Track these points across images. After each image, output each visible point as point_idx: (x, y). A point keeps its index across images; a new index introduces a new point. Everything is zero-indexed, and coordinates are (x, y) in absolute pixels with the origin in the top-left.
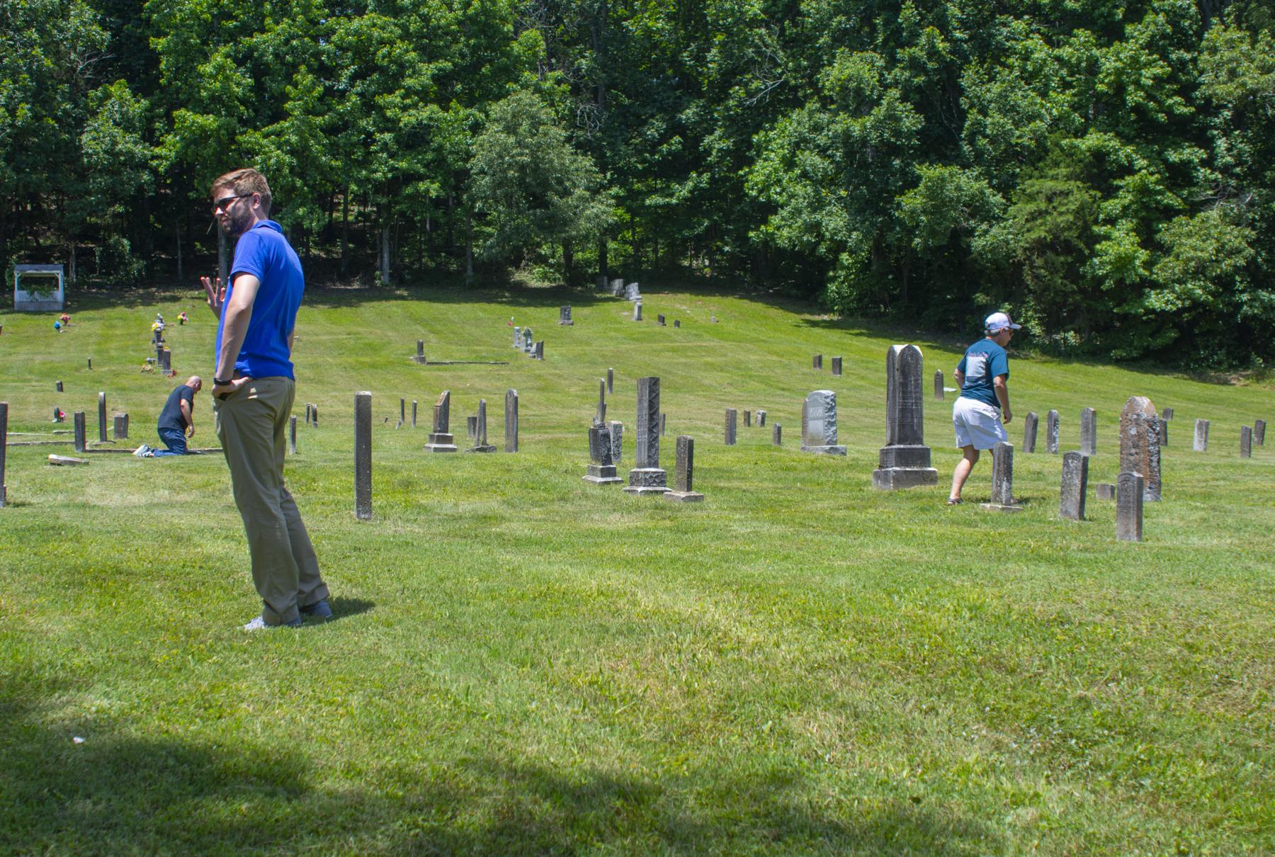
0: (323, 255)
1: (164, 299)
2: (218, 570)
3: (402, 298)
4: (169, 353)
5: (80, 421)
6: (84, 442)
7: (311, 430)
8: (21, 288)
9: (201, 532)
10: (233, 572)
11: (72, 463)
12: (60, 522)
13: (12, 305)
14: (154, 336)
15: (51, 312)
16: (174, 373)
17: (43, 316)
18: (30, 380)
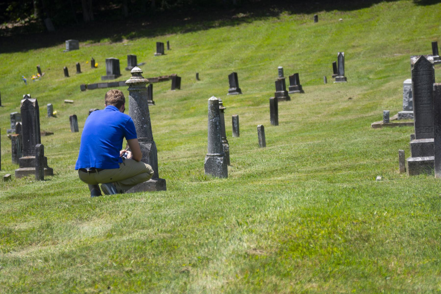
3: (243, 20)
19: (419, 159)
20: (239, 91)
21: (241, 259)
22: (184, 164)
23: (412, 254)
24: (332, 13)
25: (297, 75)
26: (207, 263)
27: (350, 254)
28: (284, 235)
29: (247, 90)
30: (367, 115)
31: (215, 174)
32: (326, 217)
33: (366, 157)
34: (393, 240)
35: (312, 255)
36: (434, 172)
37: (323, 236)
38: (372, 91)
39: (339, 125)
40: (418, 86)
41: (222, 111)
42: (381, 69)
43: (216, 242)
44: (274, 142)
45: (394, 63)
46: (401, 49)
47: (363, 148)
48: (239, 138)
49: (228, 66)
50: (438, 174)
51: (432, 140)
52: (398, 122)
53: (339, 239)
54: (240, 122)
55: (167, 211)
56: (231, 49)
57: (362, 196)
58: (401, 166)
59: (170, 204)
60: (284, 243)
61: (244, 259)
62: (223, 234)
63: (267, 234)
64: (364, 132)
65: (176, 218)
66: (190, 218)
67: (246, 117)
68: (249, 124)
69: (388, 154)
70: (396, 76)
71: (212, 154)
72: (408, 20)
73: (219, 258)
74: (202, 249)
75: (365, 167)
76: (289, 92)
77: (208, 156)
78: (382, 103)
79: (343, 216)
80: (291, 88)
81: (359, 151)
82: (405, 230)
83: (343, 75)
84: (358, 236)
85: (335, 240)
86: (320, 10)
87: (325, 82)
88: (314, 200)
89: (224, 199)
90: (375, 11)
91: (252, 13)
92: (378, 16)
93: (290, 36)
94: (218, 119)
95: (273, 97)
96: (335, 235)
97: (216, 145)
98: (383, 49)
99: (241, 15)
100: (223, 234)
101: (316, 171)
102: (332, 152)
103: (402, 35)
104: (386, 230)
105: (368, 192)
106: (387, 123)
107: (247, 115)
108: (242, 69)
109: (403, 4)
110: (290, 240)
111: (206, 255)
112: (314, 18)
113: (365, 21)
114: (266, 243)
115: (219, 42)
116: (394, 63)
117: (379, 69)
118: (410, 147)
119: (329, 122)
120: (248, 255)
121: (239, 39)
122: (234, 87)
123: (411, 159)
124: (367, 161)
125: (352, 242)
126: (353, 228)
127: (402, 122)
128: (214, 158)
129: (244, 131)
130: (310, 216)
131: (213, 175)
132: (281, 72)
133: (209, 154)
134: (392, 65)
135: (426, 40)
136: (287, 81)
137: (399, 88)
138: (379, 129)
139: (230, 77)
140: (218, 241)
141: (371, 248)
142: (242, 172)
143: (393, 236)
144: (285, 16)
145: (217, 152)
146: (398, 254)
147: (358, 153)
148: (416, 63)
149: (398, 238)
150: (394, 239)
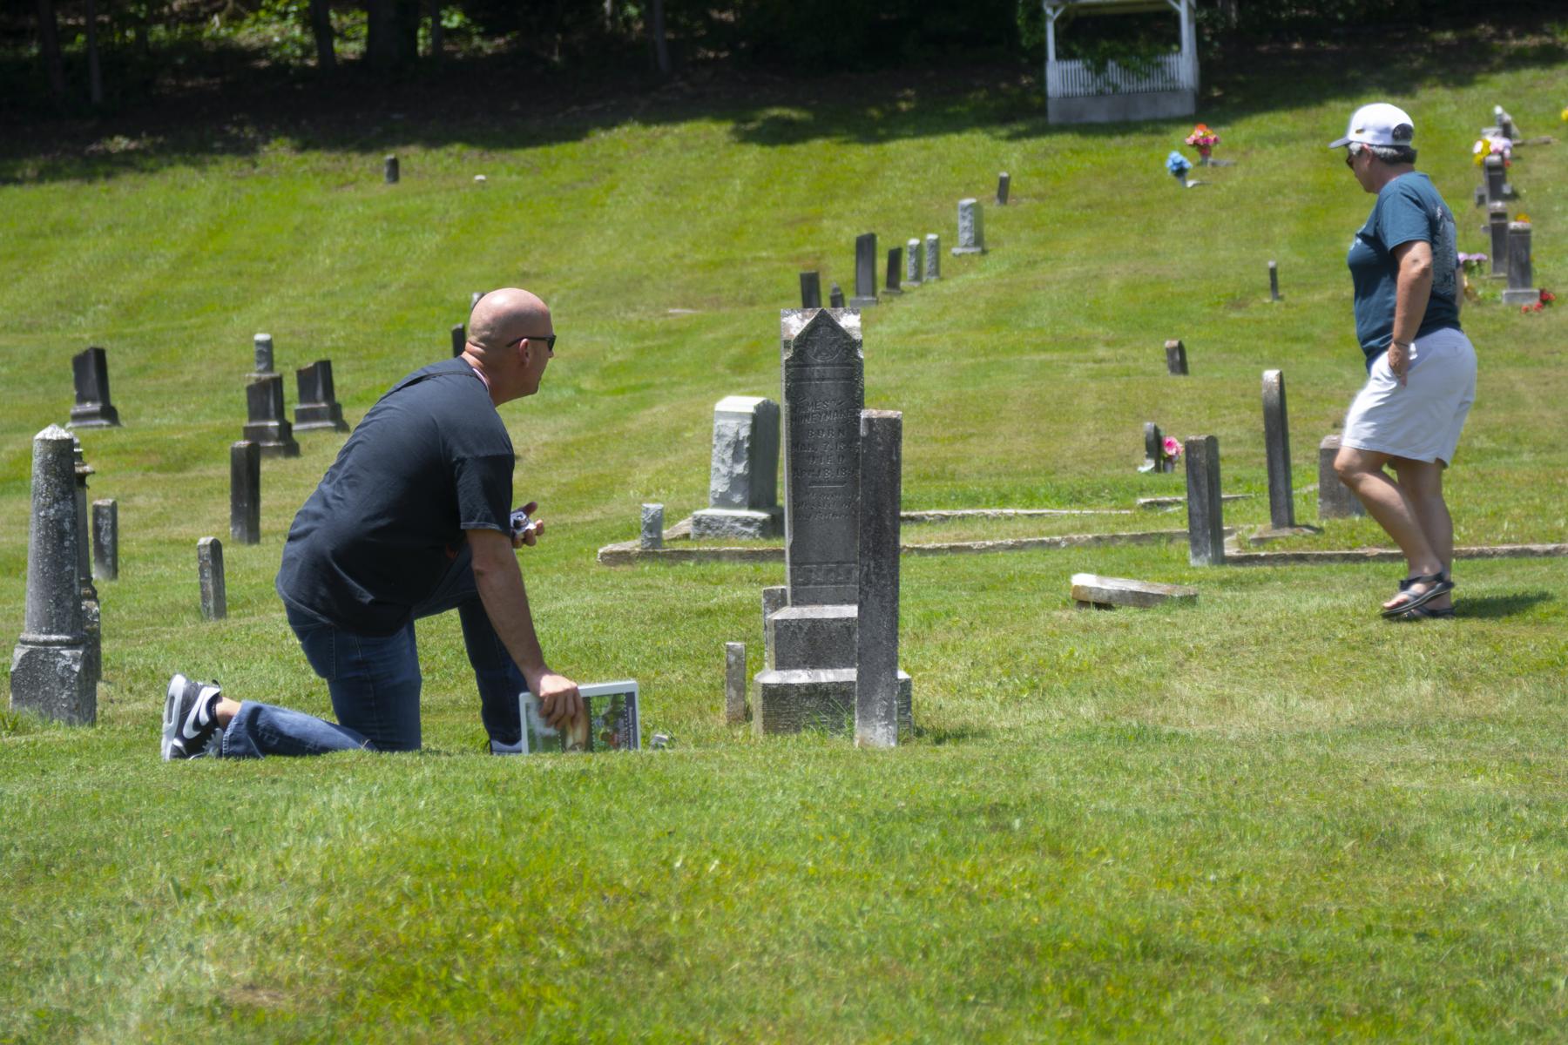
0: (715, 14)
1: (1518, 61)
2: (1479, 946)
3: (126, 162)
4: (1523, 236)
5: (1204, 467)
6: (1217, 536)
7: (248, 550)
8: (1064, 54)
9: (1460, 816)
10: (1525, 954)
11: (1142, 600)
12: (1027, 788)
13: (1042, 111)
14: (1481, 182)
15: (1158, 125)
16: (1545, 299)
17: (1135, 140)
18: (1083, 343)
19: (801, 677)
20: (109, 413)
21: (199, 1022)
23: (829, 1014)
24: (450, 155)
25: (325, 367)
26: (71, 1035)
27: (607, 1010)
28: (356, 937)
29: (138, 413)
30: (579, 519)
31: (49, 708)
32: (501, 875)
34: (754, 964)
35: (465, 1010)
36: (851, 724)
37: (499, 945)
38: (590, 434)
40: (807, 416)
41: (82, 478)
42: (620, 358)
43: (97, 957)
44: (249, 602)
45: (665, 341)
46: (691, 292)
48: (115, 584)
49: (69, 324)
50: (868, 731)
51: (851, 611)
53: (557, 956)
54: (120, 523)
56: (79, 265)
57: (618, 801)
58: (732, 701)
60: (358, 967)
61: (212, 1023)
62: (124, 929)
63: (288, 932)
64: (574, 576)
67: (138, 509)
68: (151, 534)
69: (676, 657)
70: (673, 384)
71: (43, 638)
72: (716, 192)
73: (116, 1017)
74: (47, 981)
76: (295, 427)
77: (25, 642)
78: (630, 479)
79: (564, 871)
80: (303, 410)
81: (572, 644)
82: (793, 928)
84: (626, 944)
85: (545, 958)
86: (406, 143)
88: (448, 813)
90: (602, 155)
91: (160, 139)
92: (610, 171)
93: (297, 229)
95: (243, 443)
96: (542, 939)
97: (59, 602)
98: (630, 287)
99: (122, 143)
100: (124, 929)
103: (696, 245)
104: (726, 925)
105: (638, 787)
106: (656, 552)
107: (140, 501)
108: (122, 337)
109: (697, 137)
110: (379, 956)
111: (66, 1006)
112: (386, 170)
113: (563, 186)
114: (288, 963)
116: (665, 341)
117: (612, 358)
118: (772, 633)
120: (224, 1007)
122: (93, 400)
125: (608, 967)
126: (607, 917)
128: (47, 652)
129: (132, 558)
131: (41, 715)
132: (266, 352)
133: (31, 637)
134: (659, 348)
135: (777, 265)
136: (291, 388)
137: (686, 429)
138: (624, 569)
139: (80, 362)
140: (106, 956)
141: (679, 988)
143: (753, 946)
144: (279, 154)
145: (61, 631)
146: (777, 1012)
147: (568, 649)
149: (771, 954)
150: (758, 956)
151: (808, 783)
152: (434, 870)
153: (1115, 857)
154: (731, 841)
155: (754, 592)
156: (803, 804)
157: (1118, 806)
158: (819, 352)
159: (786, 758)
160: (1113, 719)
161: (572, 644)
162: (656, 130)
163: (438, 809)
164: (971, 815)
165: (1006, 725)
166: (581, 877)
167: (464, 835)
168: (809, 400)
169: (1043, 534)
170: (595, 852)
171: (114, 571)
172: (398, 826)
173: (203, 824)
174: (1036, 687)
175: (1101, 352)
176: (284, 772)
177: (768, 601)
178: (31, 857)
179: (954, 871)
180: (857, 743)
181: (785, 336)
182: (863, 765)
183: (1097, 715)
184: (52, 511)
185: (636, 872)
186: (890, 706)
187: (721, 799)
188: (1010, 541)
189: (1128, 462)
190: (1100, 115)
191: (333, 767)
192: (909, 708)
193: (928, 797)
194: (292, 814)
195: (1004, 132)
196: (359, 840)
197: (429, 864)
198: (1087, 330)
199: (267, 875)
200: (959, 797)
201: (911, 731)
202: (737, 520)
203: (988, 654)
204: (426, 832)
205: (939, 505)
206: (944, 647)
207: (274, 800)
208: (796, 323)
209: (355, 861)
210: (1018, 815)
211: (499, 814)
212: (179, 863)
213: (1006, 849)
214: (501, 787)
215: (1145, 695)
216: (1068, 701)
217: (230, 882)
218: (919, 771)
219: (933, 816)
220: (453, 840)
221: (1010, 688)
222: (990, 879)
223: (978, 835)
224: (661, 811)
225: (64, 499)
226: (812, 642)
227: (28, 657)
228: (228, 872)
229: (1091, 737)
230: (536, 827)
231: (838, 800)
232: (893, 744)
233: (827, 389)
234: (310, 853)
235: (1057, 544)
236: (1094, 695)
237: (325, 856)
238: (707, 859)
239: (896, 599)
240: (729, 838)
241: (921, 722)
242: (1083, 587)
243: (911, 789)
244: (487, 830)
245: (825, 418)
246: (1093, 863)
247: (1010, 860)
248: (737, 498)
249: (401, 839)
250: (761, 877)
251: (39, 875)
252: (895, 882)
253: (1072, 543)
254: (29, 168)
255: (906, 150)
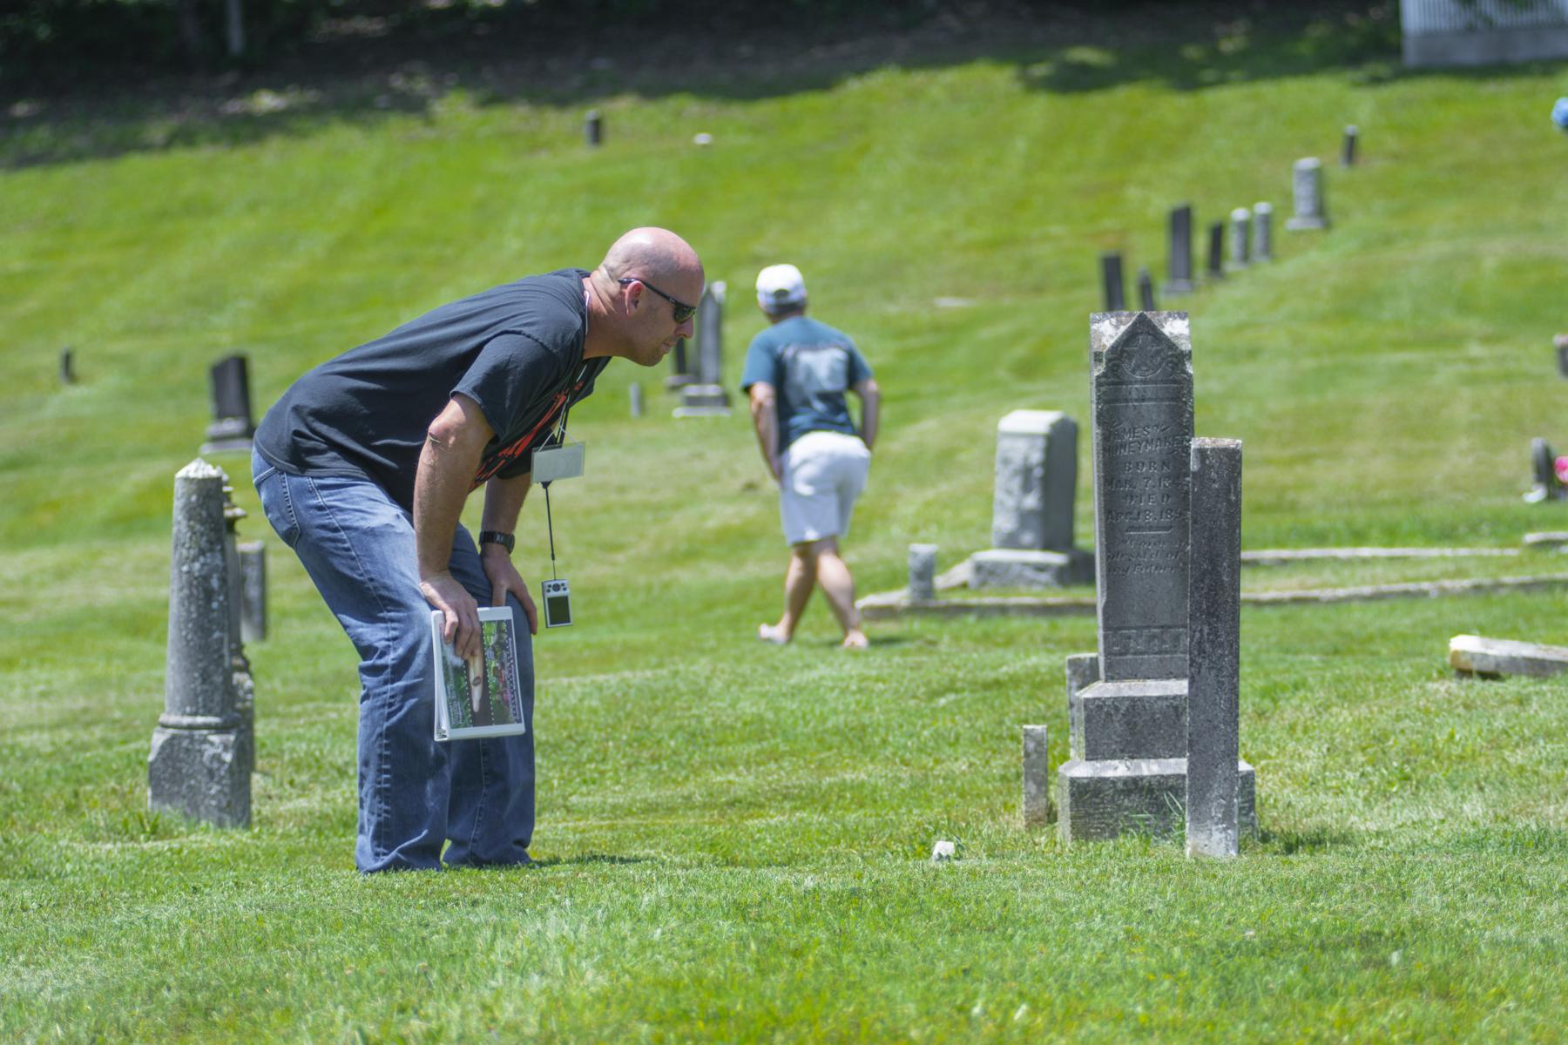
11: (1539, 669)
12: (1406, 912)
17: (1524, 84)
18: (1454, 340)
19: (1118, 769)
22: (39, 755)
31: (195, 807)
33: (865, 750)
36: (1182, 827)
39: (710, 605)
40: (1123, 446)
41: (231, 523)
47: (846, 711)
50: (1203, 836)
51: (1180, 687)
52: (973, 600)
55: (17, 973)
58: (1032, 798)
59: (29, 945)
65: (72, 1010)
66: (137, 1011)
71: (187, 720)
75: (863, 796)
77: (165, 726)
79: (836, 1019)
81: (830, 724)
83: (718, 381)
87: (633, 411)
88: (690, 945)
89: (278, 930)
94: (218, 561)
97: (205, 677)
99: (266, 101)
101: (651, 808)
102: (708, 721)
106: (926, 605)
115: (162, 215)
119: (666, 586)
121: (253, 207)
122: (233, 415)
123: (1083, 770)
124: (871, 767)
127: (989, 600)
128: (191, 738)
129: (285, 614)
130: (685, 1016)
131: (186, 815)
142: (313, 802)
144: (456, 109)
148: (1114, 348)
151: (1133, 905)
152: (679, 1018)
153: (1518, 999)
154: (1041, 980)
155: (1054, 655)
156: (1127, 932)
157: (1518, 934)
158: (1138, 367)
159: (1103, 873)
160: (1506, 820)
161: (830, 724)
162: (918, 78)
163: (678, 939)
164: (1337, 947)
165: (1373, 827)
166: (858, 1026)
167: (712, 972)
168: (1126, 425)
169: (1406, 580)
170: (874, 996)
171: (263, 631)
172: (629, 961)
173: (391, 958)
174: (1407, 778)
175: (1475, 350)
176: (487, 891)
177: (1074, 673)
178: (188, 998)
179: (1320, 1019)
180: (1188, 851)
181: (1096, 347)
182: (1199, 881)
183: (1485, 814)
184: (197, 566)
185: (925, 1020)
186: (1229, 806)
187: (1026, 929)
188: (1367, 590)
189: (1511, 487)
190: (1470, 54)
191: (545, 883)
192: (1252, 808)
193: (1283, 925)
194: (500, 945)
195: (1359, 75)
196: (582, 978)
197: (669, 1010)
198: (1457, 323)
199: (473, 1022)
200: (1321, 924)
201: (1255, 835)
202: (1025, 564)
203: (1347, 736)
204: (664, 969)
205: (1279, 543)
206: (1292, 728)
207: (477, 928)
208: (1109, 331)
209: (579, 1006)
210: (1396, 948)
211: (753, 946)
212: (366, 1008)
213: (1382, 990)
214: (753, 912)
215: (1544, 788)
216: (1449, 796)
217: (429, 1031)
218: (1270, 890)
219: (1290, 948)
220: (698, 979)
221: (1376, 780)
222: (1363, 1028)
223: (1348, 972)
224: (953, 942)
225: (211, 550)
226: (1131, 725)
227: (170, 743)
228: (427, 1019)
229: (1480, 844)
230: (799, 964)
231: (1171, 928)
232: (1233, 853)
233: (1148, 411)
234: (524, 996)
235: (1423, 594)
236: (1481, 789)
237: (543, 999)
238: (1013, 1006)
239: (1235, 673)
240: (1038, 977)
241: (1266, 824)
242: (1464, 653)
243: (1261, 913)
244: (738, 965)
245: (1146, 448)
246: (1491, 1007)
247: (1388, 1005)
248: (1028, 538)
249: (635, 977)
250: (1080, 1027)
251: (197, 1021)
252: (1246, 1032)
253: (1444, 593)
254: (157, 131)
255: (1233, 100)
